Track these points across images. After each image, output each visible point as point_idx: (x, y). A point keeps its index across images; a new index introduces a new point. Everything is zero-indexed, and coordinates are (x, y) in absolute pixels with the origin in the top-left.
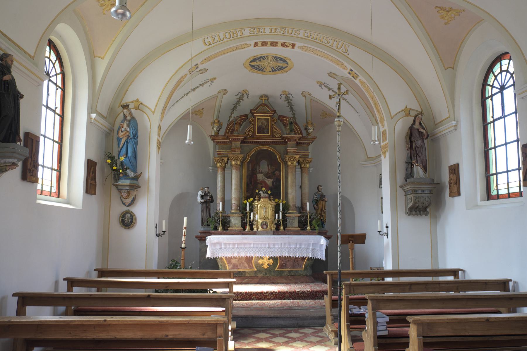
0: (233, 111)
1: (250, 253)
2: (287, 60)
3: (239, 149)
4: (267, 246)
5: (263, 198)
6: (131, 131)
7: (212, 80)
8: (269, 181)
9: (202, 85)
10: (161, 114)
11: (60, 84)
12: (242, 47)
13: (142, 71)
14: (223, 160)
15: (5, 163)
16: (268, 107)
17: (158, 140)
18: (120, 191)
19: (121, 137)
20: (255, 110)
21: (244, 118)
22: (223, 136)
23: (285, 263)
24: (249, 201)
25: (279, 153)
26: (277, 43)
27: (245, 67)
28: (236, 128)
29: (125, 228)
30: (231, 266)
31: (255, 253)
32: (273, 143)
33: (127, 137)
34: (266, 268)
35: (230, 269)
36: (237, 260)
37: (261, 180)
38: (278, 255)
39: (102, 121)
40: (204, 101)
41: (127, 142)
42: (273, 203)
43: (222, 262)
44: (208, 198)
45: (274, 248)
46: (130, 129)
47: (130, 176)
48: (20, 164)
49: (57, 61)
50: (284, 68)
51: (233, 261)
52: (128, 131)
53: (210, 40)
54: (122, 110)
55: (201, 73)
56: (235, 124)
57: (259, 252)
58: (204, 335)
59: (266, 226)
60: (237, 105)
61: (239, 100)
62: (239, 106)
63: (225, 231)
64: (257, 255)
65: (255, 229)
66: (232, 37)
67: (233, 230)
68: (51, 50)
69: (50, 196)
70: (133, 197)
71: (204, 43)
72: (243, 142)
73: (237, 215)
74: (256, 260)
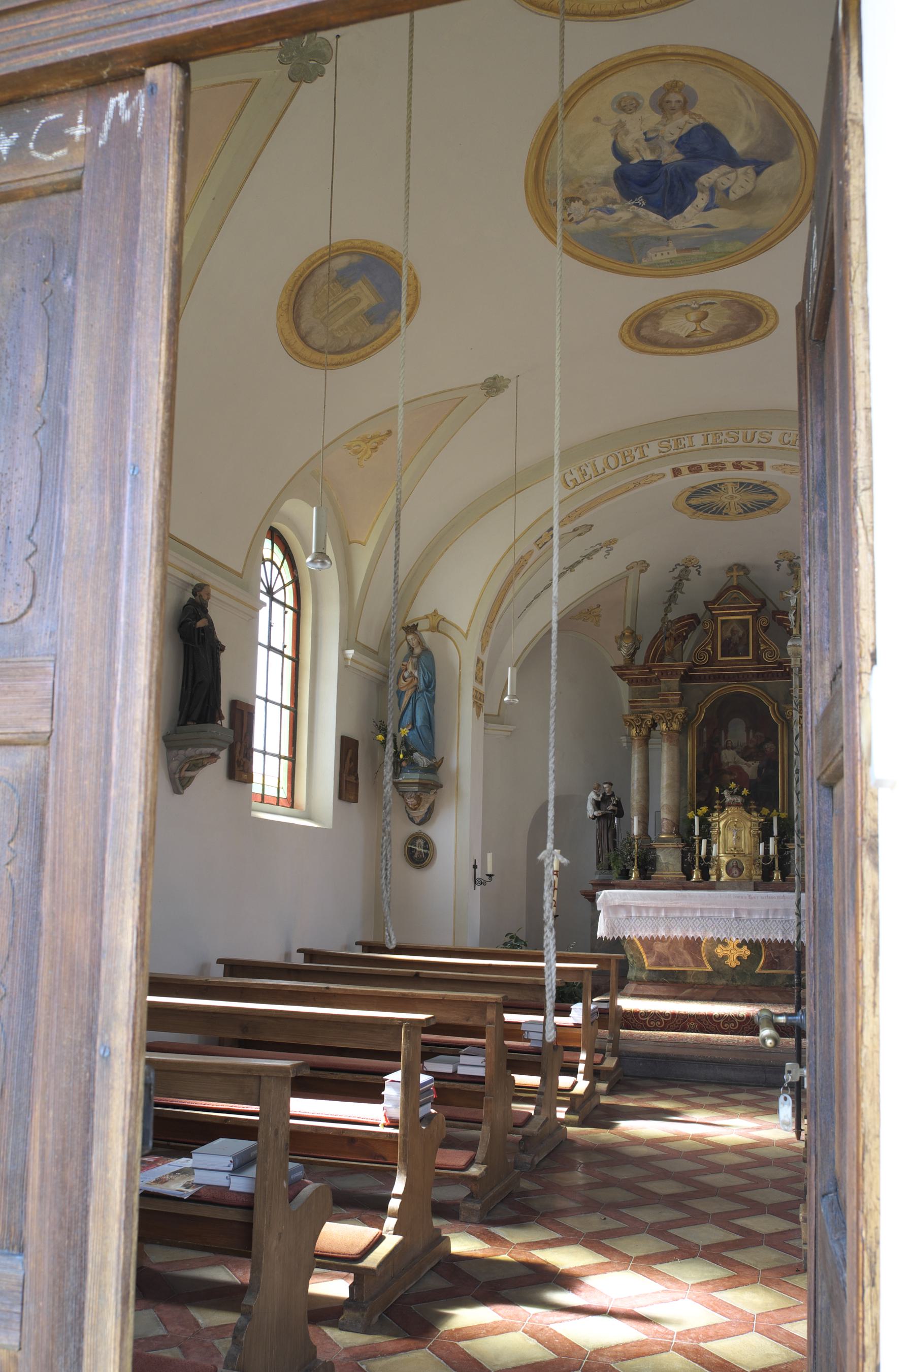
0: (670, 605)
1: (694, 931)
2: (771, 487)
3: (675, 695)
4: (733, 915)
5: (730, 805)
6: (421, 677)
7: (609, 545)
8: (749, 766)
9: (588, 557)
10: (482, 637)
11: (290, 602)
12: (647, 480)
13: (443, 554)
14: (643, 720)
15: (201, 754)
16: (746, 592)
17: (475, 691)
18: (402, 794)
19: (403, 690)
20: (713, 602)
21: (692, 621)
22: (641, 666)
23: (777, 958)
24: (700, 812)
25: (773, 699)
26: (723, 464)
27: (680, 511)
28: (667, 649)
29: (414, 867)
30: (653, 959)
31: (706, 931)
32: (758, 677)
33: (414, 689)
34: (733, 965)
35: (652, 965)
36: (666, 944)
37: (730, 764)
38: (760, 937)
39: (368, 661)
40: (598, 589)
41: (413, 700)
42: (755, 817)
43: (633, 949)
44: (610, 807)
45: (749, 919)
46: (419, 674)
47: (421, 765)
48: (224, 755)
49: (285, 561)
50: (770, 503)
51: (659, 947)
52: (415, 677)
53: (577, 475)
54: (404, 638)
55: (580, 535)
56: (666, 638)
57: (713, 929)
58: (468, 1020)
59: (737, 872)
60: (678, 593)
61: (680, 580)
62: (682, 593)
63: (643, 881)
64: (710, 935)
65: (713, 878)
66: (621, 463)
67: (662, 879)
68: (275, 545)
69: (278, 804)
70: (427, 806)
71: (565, 484)
72: (687, 677)
73: (670, 845)
74: (710, 948)
